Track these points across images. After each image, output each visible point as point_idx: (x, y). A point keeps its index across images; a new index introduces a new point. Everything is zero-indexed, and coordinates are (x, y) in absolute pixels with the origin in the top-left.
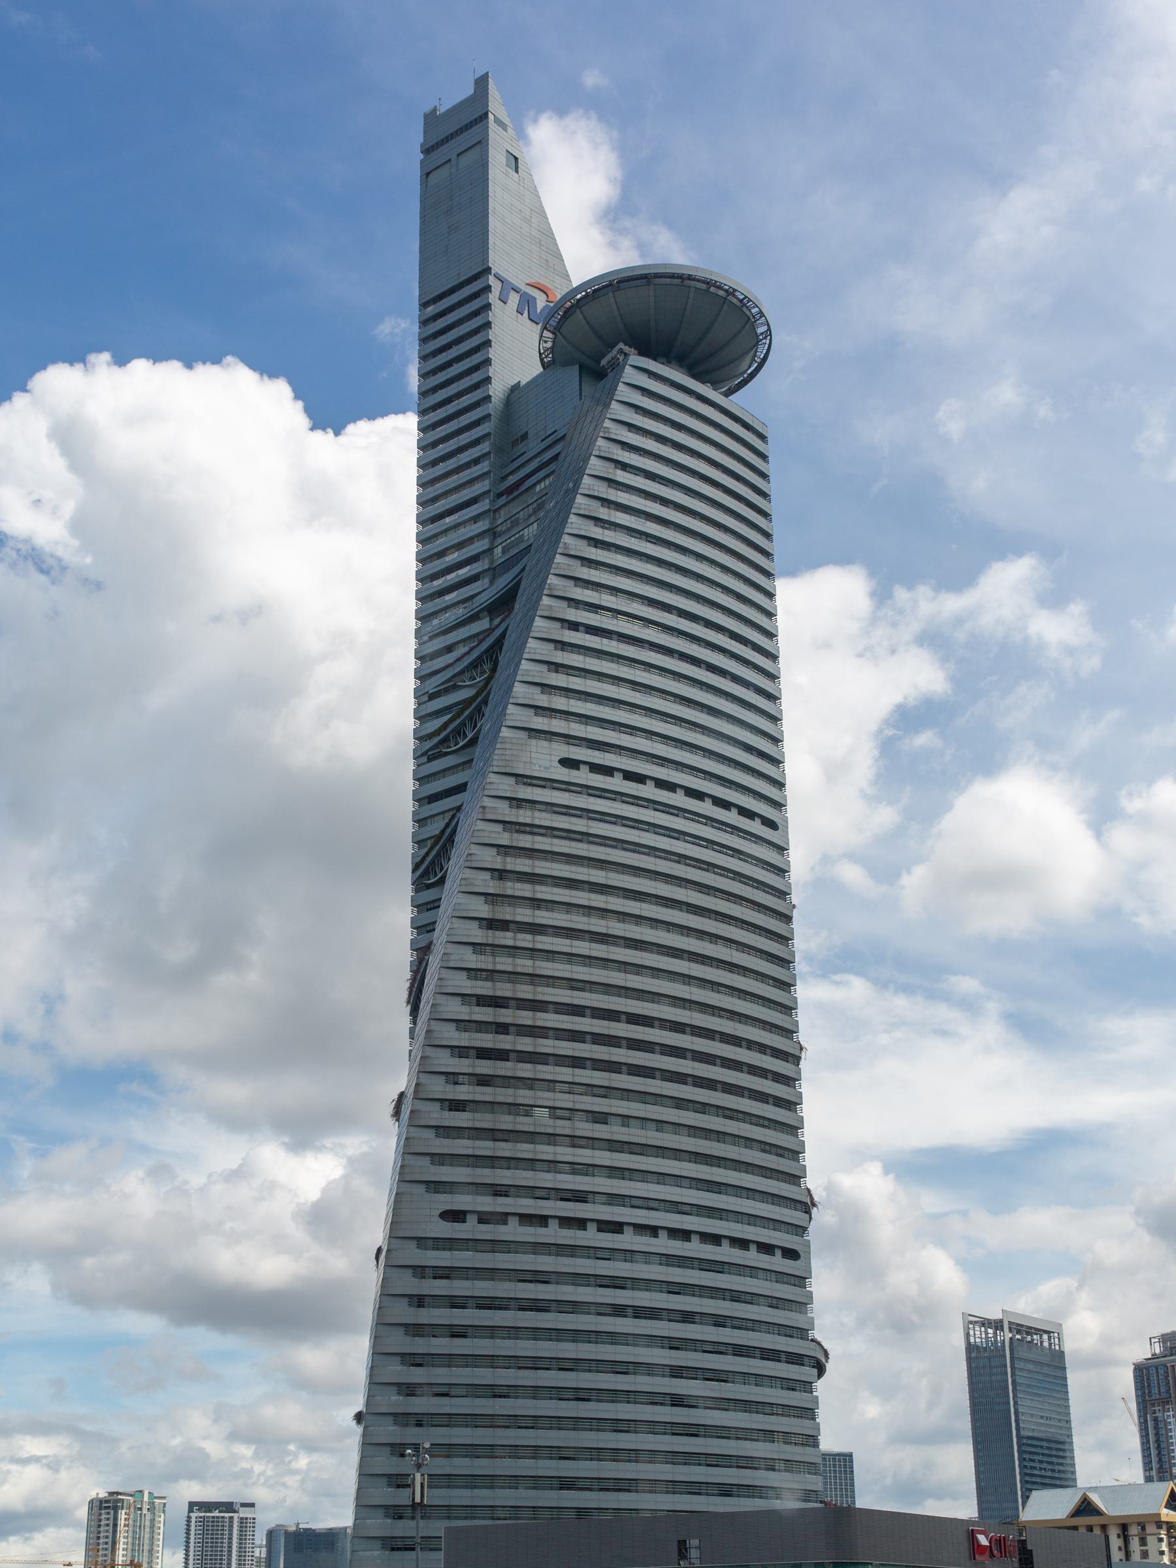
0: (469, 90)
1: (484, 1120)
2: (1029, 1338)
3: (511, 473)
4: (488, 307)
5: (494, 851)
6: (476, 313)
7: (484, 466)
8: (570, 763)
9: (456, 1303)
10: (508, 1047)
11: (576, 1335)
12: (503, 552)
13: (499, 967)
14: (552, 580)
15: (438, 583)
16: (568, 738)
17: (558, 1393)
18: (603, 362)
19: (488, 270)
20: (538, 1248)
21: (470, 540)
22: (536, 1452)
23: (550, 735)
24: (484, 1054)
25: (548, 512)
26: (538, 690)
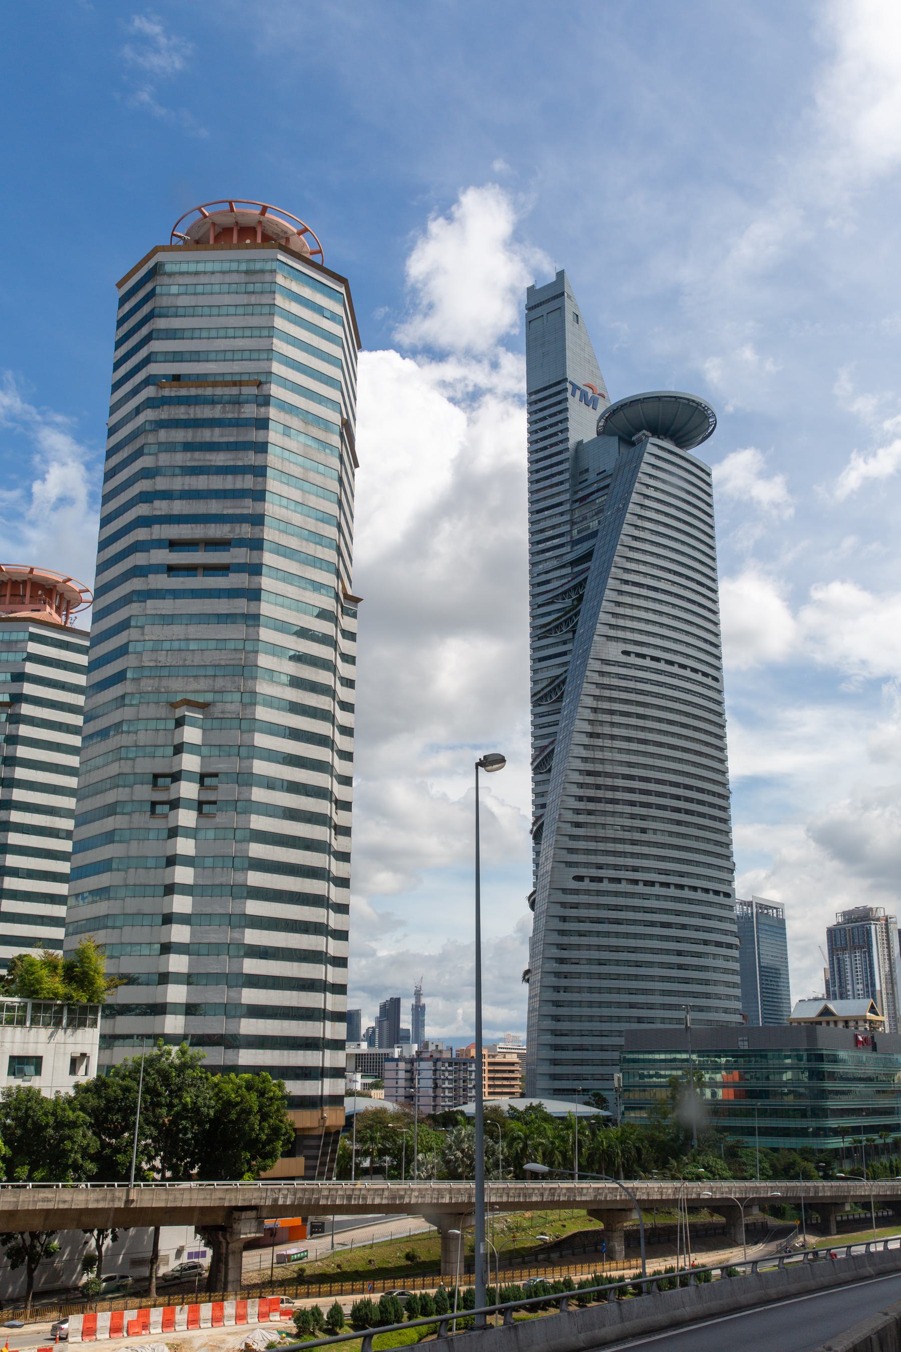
0: (553, 278)
1: (591, 832)
2: (766, 911)
3: (581, 490)
4: (566, 399)
5: (592, 698)
6: (560, 403)
8: (626, 653)
9: (580, 920)
10: (601, 796)
11: (636, 936)
12: (578, 533)
13: (597, 757)
14: (616, 558)
15: (542, 546)
16: (625, 640)
17: (628, 963)
18: (634, 438)
19: (565, 380)
20: (616, 894)
21: (559, 525)
22: (619, 991)
23: (617, 639)
24: (590, 799)
25: (606, 517)
26: (610, 616)
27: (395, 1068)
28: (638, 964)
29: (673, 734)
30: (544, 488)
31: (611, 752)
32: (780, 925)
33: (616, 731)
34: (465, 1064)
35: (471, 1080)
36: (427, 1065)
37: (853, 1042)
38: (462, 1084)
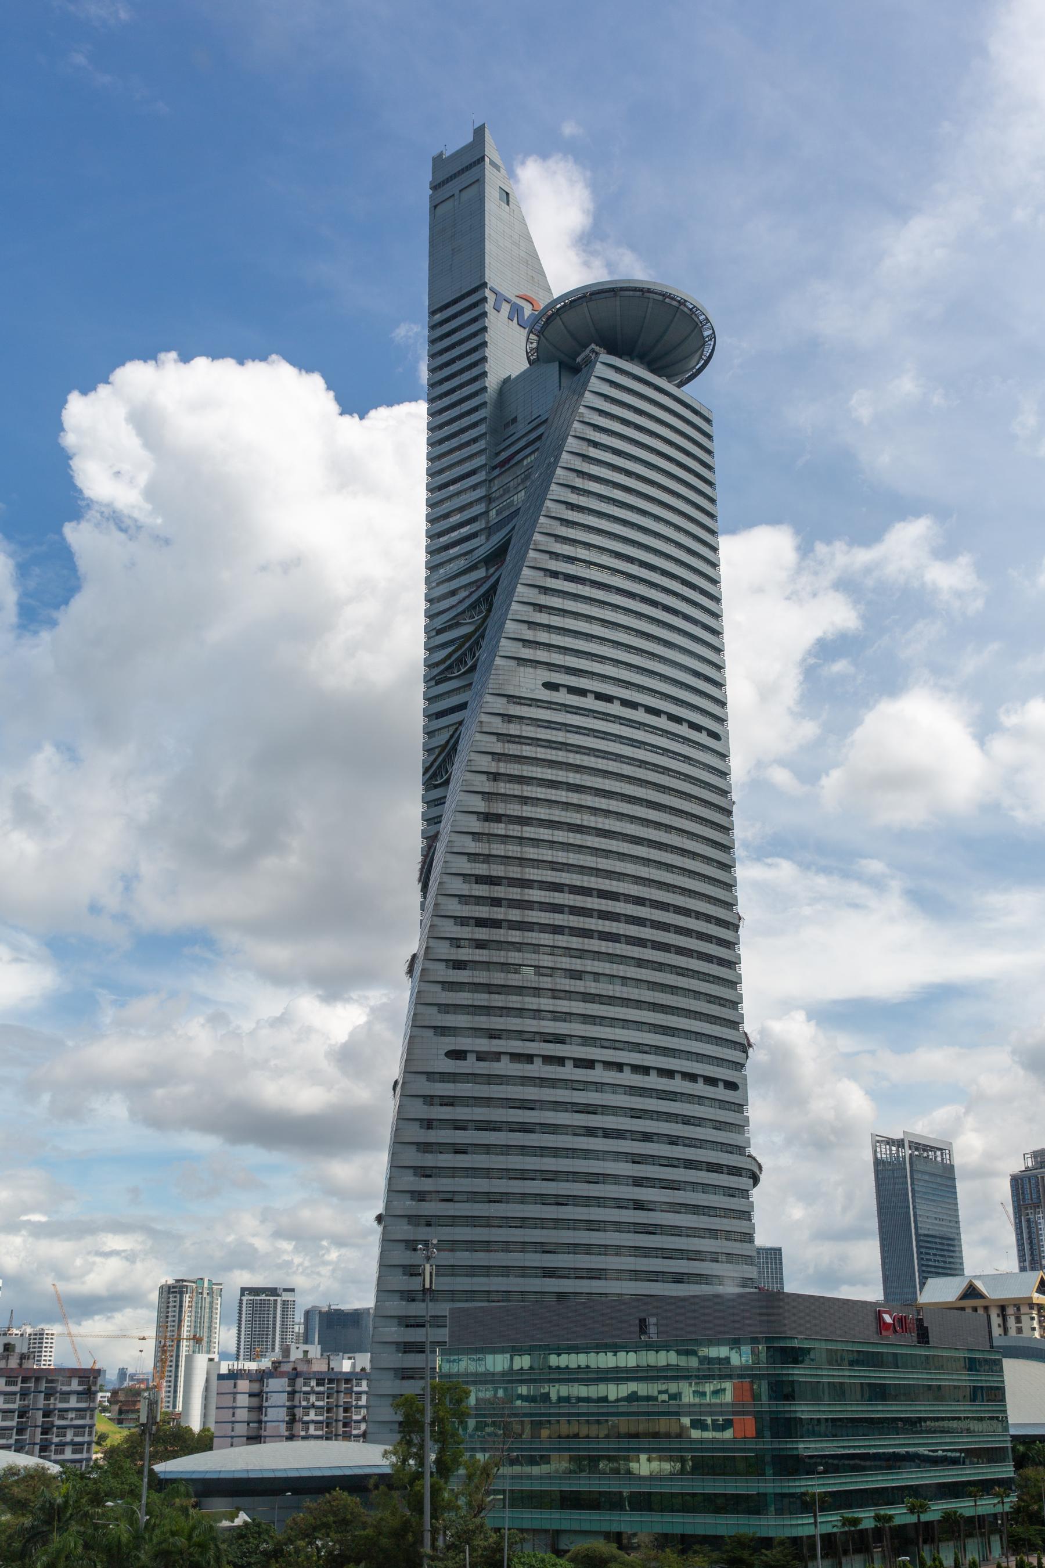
0: (470, 138)
1: (481, 977)
2: (925, 1154)
3: (503, 450)
4: (484, 314)
7: (481, 444)
8: (550, 686)
9: (459, 1125)
10: (501, 917)
12: (497, 515)
13: (494, 852)
14: (537, 537)
16: (550, 666)
17: (541, 1199)
18: (579, 360)
20: (525, 1081)
21: (470, 505)
23: (535, 663)
24: (481, 922)
27: (232, 1390)
28: (560, 1201)
31: (520, 845)
34: (348, 1381)
35: (358, 1407)
36: (277, 1385)
38: (341, 1415)
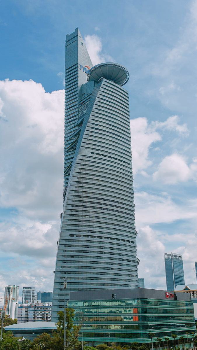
1: (77, 218)
8: (92, 153)
11: (94, 257)
17: (90, 268)
18: (99, 80)
19: (78, 64)
24: (77, 206)
29: (111, 183)
30: (70, 101)
31: (86, 188)
32: (181, 262)
33: (88, 181)
34: (47, 308)
36: (31, 309)
37: (164, 296)
38: (46, 316)
